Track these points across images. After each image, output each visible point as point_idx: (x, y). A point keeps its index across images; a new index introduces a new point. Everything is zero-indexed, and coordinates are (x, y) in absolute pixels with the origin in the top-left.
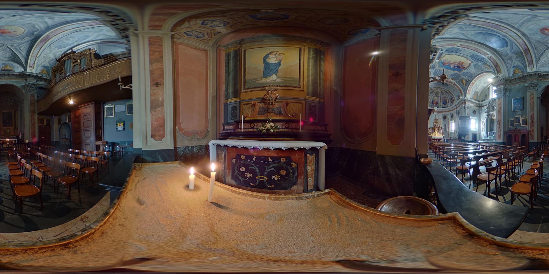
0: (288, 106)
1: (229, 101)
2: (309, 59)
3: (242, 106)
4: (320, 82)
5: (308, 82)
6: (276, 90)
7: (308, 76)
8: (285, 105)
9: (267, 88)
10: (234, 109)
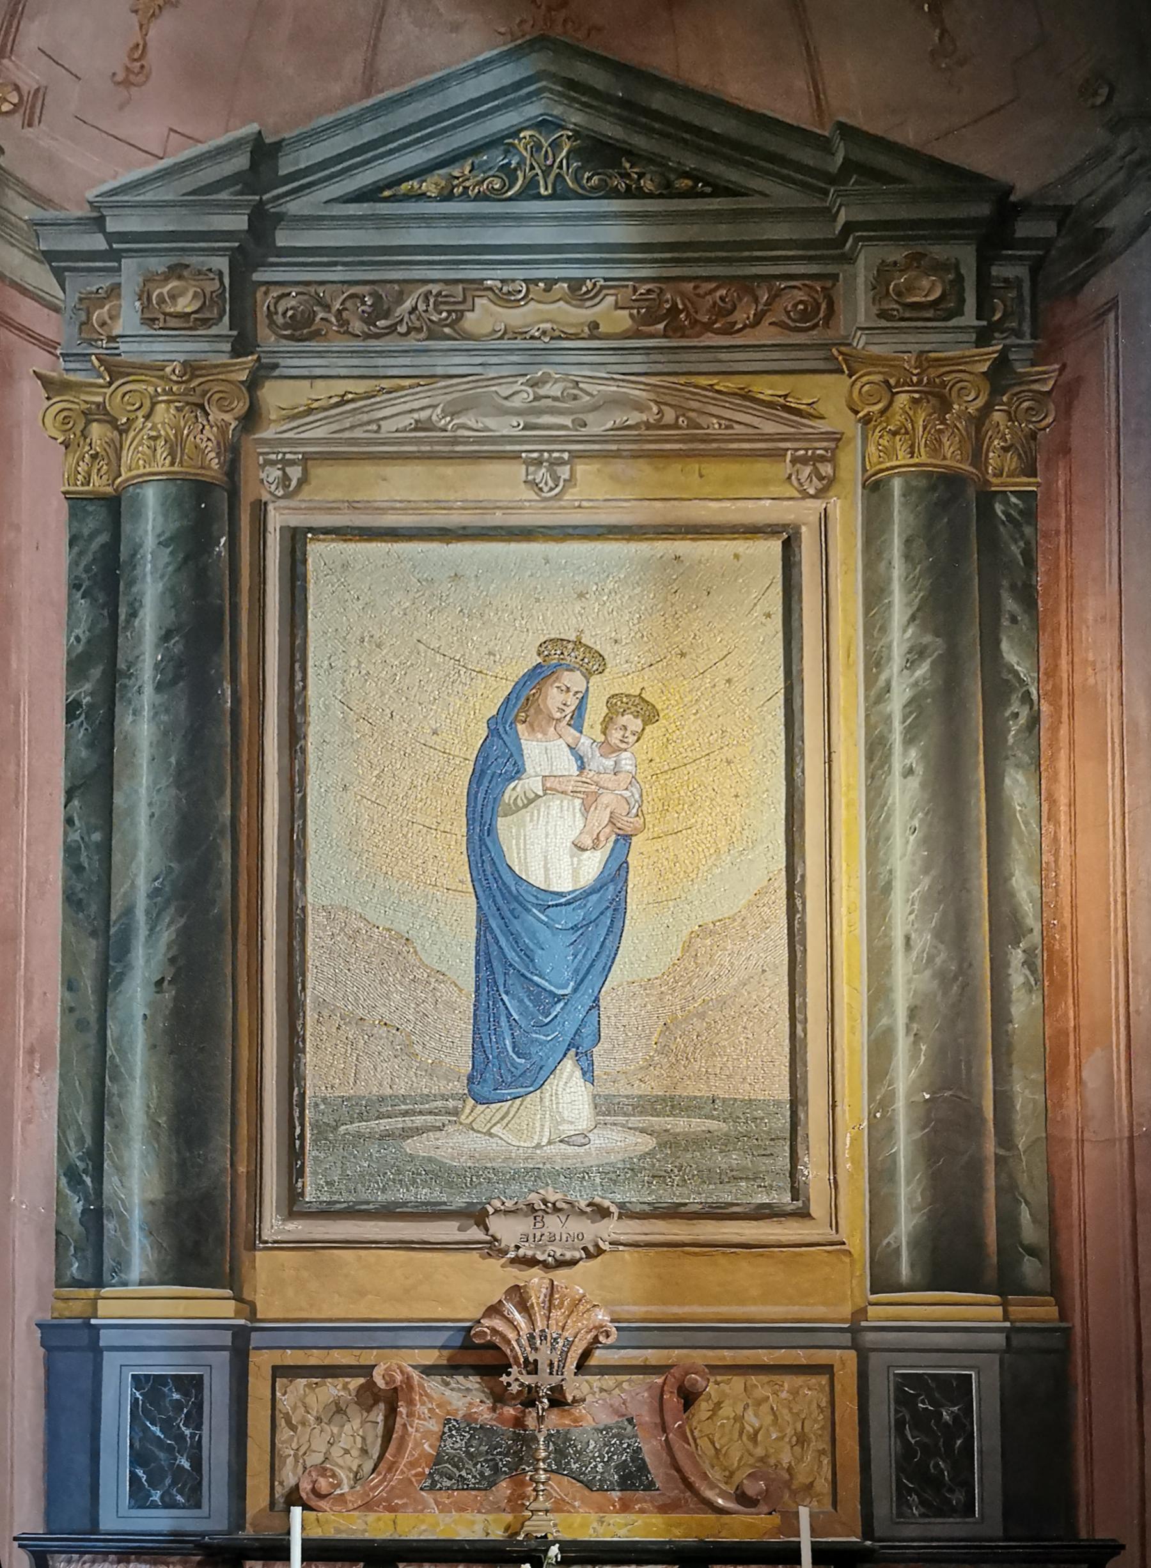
0: (703, 1408)
1: (112, 1308)
2: (875, 595)
3: (259, 1387)
4: (1003, 1101)
5: (879, 1133)
6: (593, 1253)
7: (880, 1050)
8: (673, 1400)
9: (507, 1230)
10: (169, 1401)
